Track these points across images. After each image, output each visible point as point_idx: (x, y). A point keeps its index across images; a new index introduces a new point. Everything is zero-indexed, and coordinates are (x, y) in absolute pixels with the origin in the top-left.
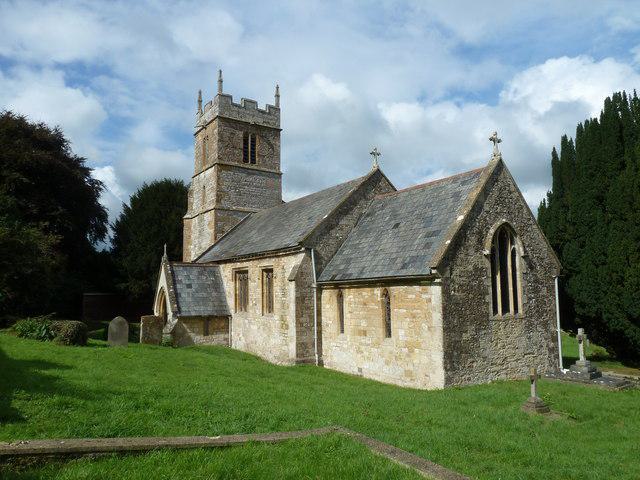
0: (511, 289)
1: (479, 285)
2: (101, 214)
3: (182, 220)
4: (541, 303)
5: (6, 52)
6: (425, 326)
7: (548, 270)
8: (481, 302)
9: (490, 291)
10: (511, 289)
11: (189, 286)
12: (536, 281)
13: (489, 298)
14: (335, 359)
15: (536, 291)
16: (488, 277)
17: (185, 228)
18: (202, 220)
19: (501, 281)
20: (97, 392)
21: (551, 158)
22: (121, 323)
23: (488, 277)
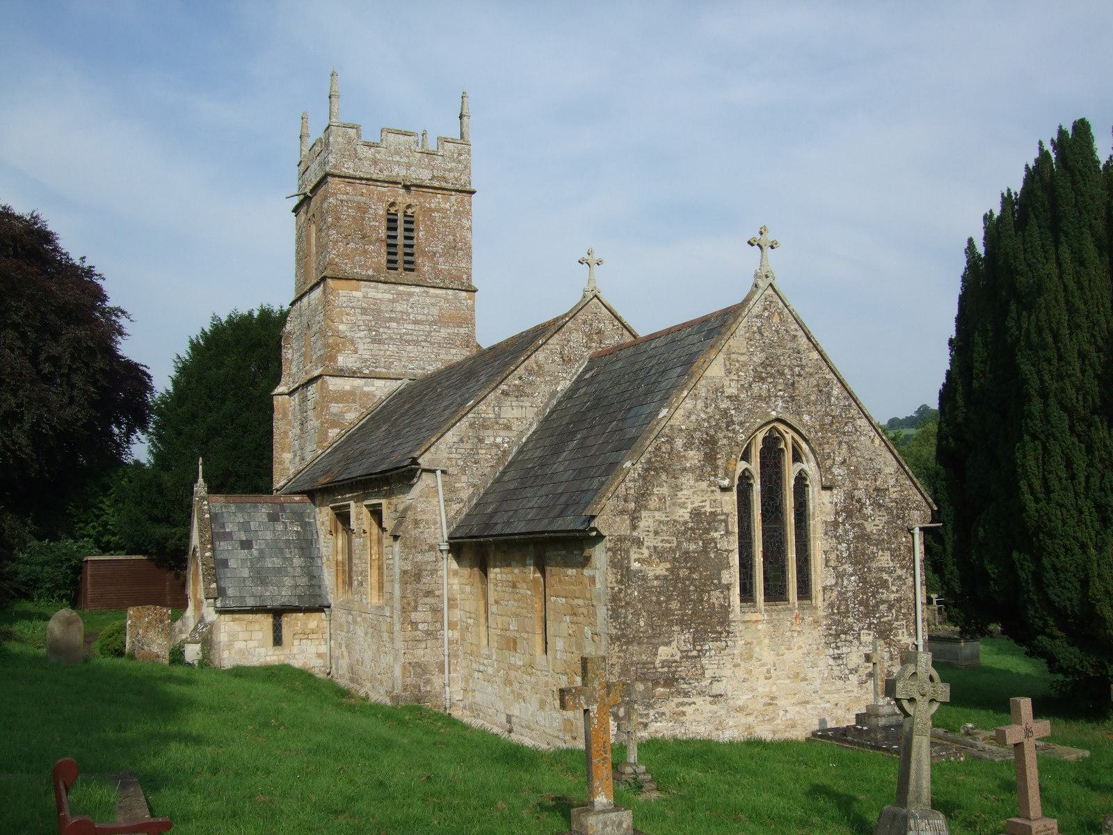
0: (759, 560)
1: (705, 551)
2: (136, 377)
3: (271, 398)
4: (870, 586)
5: (631, 832)
6: (588, 631)
7: (899, 512)
8: (712, 581)
9: (735, 560)
10: (759, 560)
11: (246, 545)
12: (863, 537)
13: (732, 576)
14: (466, 572)
15: (860, 559)
16: (728, 533)
17: (276, 415)
18: (304, 400)
19: (797, 527)
20: (1051, 332)
21: (966, 245)
22: (68, 622)
23: (728, 533)
